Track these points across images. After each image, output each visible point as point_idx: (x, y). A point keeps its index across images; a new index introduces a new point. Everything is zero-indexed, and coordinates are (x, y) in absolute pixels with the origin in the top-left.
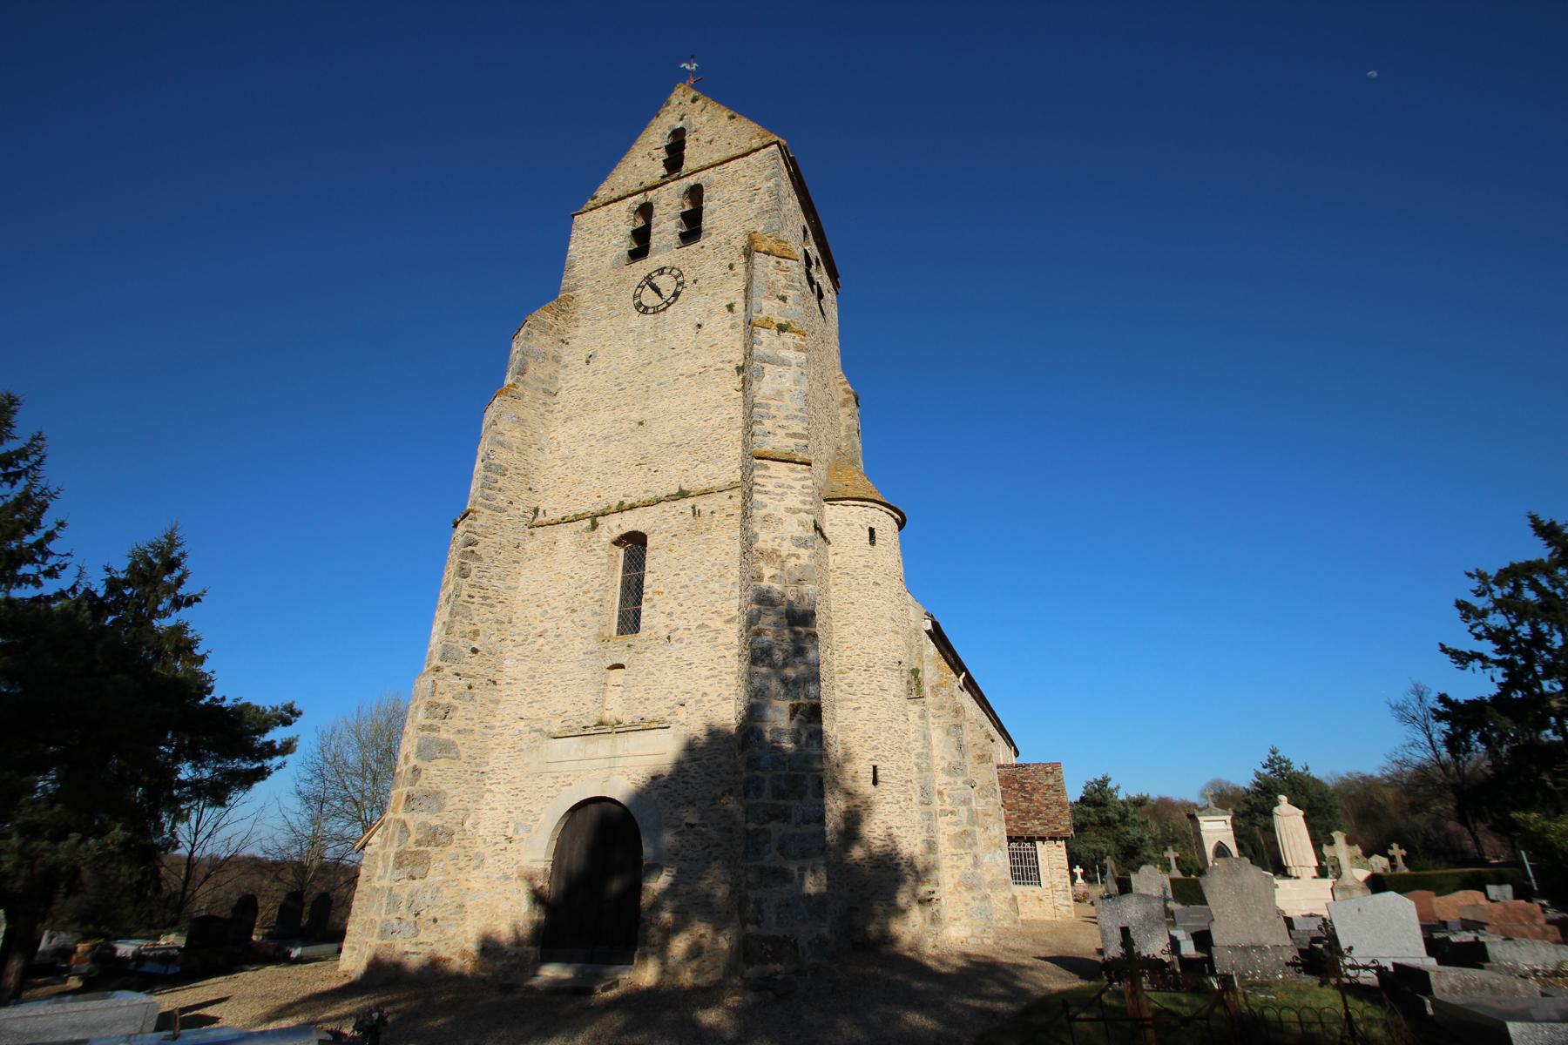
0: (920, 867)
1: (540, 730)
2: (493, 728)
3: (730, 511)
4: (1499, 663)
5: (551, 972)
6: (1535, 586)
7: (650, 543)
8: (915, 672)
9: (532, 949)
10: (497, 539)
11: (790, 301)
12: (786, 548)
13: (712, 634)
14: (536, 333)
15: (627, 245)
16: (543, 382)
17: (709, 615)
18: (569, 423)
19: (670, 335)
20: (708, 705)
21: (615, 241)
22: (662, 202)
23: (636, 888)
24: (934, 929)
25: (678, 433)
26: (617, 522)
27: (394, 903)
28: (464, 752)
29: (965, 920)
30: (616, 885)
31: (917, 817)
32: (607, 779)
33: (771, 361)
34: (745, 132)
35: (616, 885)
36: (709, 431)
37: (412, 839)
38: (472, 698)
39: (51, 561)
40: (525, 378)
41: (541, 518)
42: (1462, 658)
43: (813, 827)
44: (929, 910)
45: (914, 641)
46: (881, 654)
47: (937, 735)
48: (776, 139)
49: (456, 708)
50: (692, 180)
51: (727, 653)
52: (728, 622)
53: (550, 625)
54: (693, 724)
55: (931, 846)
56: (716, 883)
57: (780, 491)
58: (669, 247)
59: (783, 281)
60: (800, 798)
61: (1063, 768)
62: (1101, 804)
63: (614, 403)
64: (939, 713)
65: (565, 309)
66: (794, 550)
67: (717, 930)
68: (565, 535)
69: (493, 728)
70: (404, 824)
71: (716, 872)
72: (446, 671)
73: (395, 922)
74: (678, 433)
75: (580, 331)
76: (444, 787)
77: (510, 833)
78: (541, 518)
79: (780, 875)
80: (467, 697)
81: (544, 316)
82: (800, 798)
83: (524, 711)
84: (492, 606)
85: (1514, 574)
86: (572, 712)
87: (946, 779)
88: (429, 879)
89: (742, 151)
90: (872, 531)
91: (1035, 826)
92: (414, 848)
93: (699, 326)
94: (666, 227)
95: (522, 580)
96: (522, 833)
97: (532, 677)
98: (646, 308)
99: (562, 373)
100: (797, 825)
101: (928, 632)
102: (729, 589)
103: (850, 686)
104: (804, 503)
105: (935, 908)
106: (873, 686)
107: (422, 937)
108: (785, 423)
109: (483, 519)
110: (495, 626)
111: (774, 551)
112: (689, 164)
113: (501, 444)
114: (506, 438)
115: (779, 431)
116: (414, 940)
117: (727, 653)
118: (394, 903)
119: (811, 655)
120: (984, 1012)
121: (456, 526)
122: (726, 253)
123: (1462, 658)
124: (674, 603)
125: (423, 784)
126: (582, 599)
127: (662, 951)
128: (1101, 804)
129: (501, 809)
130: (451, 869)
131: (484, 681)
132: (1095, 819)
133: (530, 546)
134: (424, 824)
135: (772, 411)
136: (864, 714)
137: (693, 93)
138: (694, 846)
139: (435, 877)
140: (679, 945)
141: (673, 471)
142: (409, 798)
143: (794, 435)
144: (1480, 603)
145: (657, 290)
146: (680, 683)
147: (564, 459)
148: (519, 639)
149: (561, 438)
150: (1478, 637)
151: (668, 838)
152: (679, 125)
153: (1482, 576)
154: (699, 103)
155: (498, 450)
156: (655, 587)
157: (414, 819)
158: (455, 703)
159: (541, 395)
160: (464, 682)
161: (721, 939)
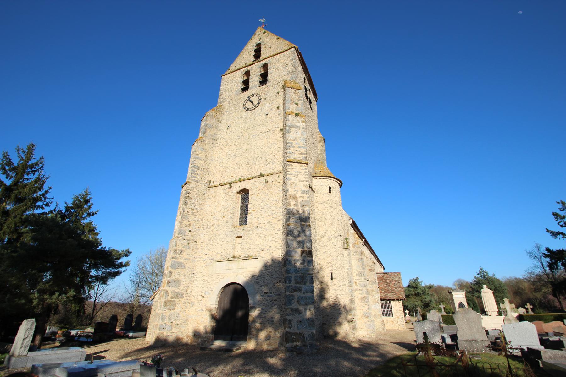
0: (348, 308)
2: (197, 258)
5: (218, 343)
9: (211, 335)
10: (197, 192)
14: (209, 118)
16: (212, 136)
17: (271, 218)
19: (256, 118)
21: (237, 85)
22: (253, 70)
23: (247, 315)
24: (354, 332)
27: (164, 318)
28: (187, 266)
31: (347, 291)
34: (283, 44)
35: (240, 313)
37: (170, 296)
38: (189, 248)
39: (47, 200)
40: (206, 135)
41: (212, 184)
44: (352, 325)
45: (346, 228)
46: (333, 232)
48: (294, 46)
49: (184, 251)
50: (264, 62)
51: (278, 232)
52: (278, 221)
54: (266, 257)
55: (352, 301)
57: (296, 174)
59: (297, 98)
60: (305, 284)
61: (401, 274)
62: (415, 288)
63: (237, 143)
64: (355, 254)
66: (302, 195)
68: (221, 190)
69: (197, 258)
72: (180, 238)
73: (164, 325)
75: (225, 118)
76: (180, 278)
77: (203, 295)
78: (212, 184)
79: (298, 311)
81: (212, 112)
82: (305, 284)
83: (207, 252)
87: (358, 278)
88: (176, 310)
90: (330, 188)
91: (390, 295)
92: (170, 300)
94: (255, 79)
96: (207, 295)
97: (210, 240)
99: (219, 133)
100: (304, 293)
101: (351, 225)
102: (279, 209)
103: (322, 244)
104: (305, 178)
105: (354, 324)
106: (331, 244)
107: (174, 330)
108: (298, 149)
109: (192, 185)
112: (263, 56)
113: (198, 158)
114: (200, 156)
115: (296, 152)
117: (278, 232)
118: (164, 318)
125: (173, 277)
127: (256, 337)
128: (415, 288)
131: (193, 242)
132: (413, 293)
133: (208, 194)
134: (173, 291)
135: (294, 145)
136: (327, 254)
137: (264, 30)
139: (177, 309)
140: (262, 335)
142: (168, 282)
143: (302, 154)
145: (252, 102)
148: (205, 227)
149: (218, 156)
150: (562, 226)
151: (258, 297)
152: (259, 42)
154: (266, 34)
155: (197, 160)
156: (252, 208)
157: (170, 289)
158: (184, 249)
159: (211, 141)
160: (187, 242)
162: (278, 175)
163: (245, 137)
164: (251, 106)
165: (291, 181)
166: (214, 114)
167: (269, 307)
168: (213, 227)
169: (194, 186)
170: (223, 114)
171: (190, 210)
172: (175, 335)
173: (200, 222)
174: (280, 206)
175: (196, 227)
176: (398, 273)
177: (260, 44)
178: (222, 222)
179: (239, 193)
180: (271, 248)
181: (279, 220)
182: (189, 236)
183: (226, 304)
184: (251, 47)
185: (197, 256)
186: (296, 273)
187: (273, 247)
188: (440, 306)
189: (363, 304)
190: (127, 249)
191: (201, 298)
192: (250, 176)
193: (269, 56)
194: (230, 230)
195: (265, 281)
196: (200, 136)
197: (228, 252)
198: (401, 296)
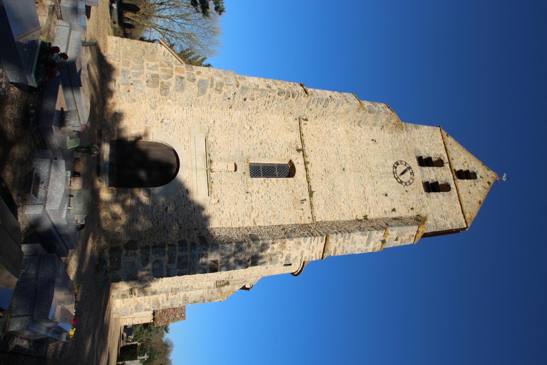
0: (146, 289)
1: (209, 132)
2: (211, 108)
3: (303, 218)
5: (106, 149)
8: (228, 283)
9: (116, 137)
10: (295, 106)
11: (395, 242)
12: (286, 252)
13: (249, 213)
14: (387, 116)
15: (425, 155)
16: (365, 120)
18: (345, 133)
19: (383, 181)
20: (218, 214)
21: (427, 149)
22: (443, 171)
23: (141, 185)
24: (120, 296)
25: (339, 189)
26: (300, 162)
27: (137, 75)
28: (201, 98)
29: (123, 305)
30: (143, 174)
31: (166, 287)
32: (187, 167)
33: (369, 239)
34: (472, 210)
35: (143, 174)
36: (339, 204)
37: (164, 80)
40: (367, 113)
41: (303, 122)
43: (166, 273)
44: (128, 293)
45: (241, 281)
47: (201, 292)
48: (469, 225)
50: (453, 186)
51: (240, 221)
52: (254, 221)
53: (255, 132)
54: (210, 210)
55: (154, 293)
56: (144, 224)
57: (311, 248)
58: (423, 176)
60: (178, 267)
61: (183, 321)
63: (353, 155)
65: (398, 127)
66: (285, 255)
67: (123, 226)
68: (294, 136)
69: (211, 108)
70: (170, 77)
71: (147, 223)
72: (237, 89)
73: (129, 76)
74: (339, 188)
75: (387, 135)
76: (186, 91)
78: (303, 122)
79: (146, 262)
80: (225, 98)
81: (395, 118)
82: (178, 267)
83: (218, 122)
84: (265, 105)
86: (217, 147)
87: (182, 296)
89: (464, 208)
92: (160, 81)
93: (386, 195)
94: (432, 174)
95: (276, 116)
97: (232, 124)
98: (396, 167)
99: (368, 127)
100: (166, 267)
102: (269, 220)
104: (306, 258)
105: (129, 296)
107: (122, 87)
108: (341, 246)
109: (304, 99)
110: (255, 107)
111: (285, 248)
112: (460, 182)
113: (338, 105)
115: (338, 244)
116: (121, 84)
117: (240, 221)
118: (137, 75)
119: (239, 267)
121: (301, 85)
122: (419, 206)
124: (263, 194)
125: (187, 83)
126: (266, 148)
127: (116, 201)
129: (175, 115)
130: (151, 96)
131: (231, 104)
133: (291, 118)
134: (170, 84)
135: (346, 241)
137: (492, 182)
138: (158, 212)
139: (147, 90)
140: (117, 209)
141: (321, 187)
142: (182, 78)
145: (402, 173)
146: (228, 199)
147: (329, 132)
148: (249, 117)
149: (339, 129)
151: (162, 199)
152: (478, 176)
154: (488, 185)
155: (335, 104)
156: (271, 184)
157: (173, 81)
158: (223, 93)
161: (119, 228)
162: (311, 216)
163: (361, 166)
165: (302, 242)
166: (392, 121)
168: (248, 128)
169: (300, 104)
170: (392, 133)
171: (272, 98)
172: (116, 88)
173: (256, 111)
174: (273, 222)
175: (250, 106)
176: (184, 318)
177: (475, 178)
178: (255, 141)
179: (291, 161)
180: (221, 212)
181: (255, 223)
182: (239, 99)
183: (155, 154)
184: (473, 165)
185: (213, 108)
186: (191, 256)
187: (222, 217)
188: (146, 355)
189: (151, 303)
190: (225, 10)
191: (160, 119)
192: (311, 177)
193: (460, 192)
194: (244, 153)
195: (181, 207)
196: (366, 104)
197: (217, 153)
198: (158, 323)
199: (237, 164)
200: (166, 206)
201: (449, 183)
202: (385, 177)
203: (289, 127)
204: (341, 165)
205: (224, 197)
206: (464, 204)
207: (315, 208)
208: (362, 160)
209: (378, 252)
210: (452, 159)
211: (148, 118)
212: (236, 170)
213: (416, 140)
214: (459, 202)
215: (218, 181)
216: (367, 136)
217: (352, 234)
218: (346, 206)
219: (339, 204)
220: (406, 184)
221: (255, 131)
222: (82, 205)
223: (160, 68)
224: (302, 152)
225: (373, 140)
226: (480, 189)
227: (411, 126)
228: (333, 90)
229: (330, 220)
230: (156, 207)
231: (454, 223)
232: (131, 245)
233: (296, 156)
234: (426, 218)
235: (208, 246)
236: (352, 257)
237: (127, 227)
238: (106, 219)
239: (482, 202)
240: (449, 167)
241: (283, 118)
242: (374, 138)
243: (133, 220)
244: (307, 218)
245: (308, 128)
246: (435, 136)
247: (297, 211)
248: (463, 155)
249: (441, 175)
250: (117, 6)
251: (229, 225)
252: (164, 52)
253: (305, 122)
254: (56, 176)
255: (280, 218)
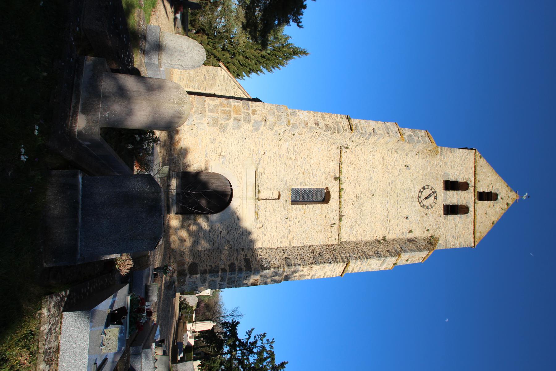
3: (330, 239)
4: (247, 342)
6: (267, 358)
7: (325, 206)
10: (338, 138)
13: (286, 236)
15: (452, 178)
17: (293, 234)
18: (381, 159)
19: (407, 205)
21: (456, 173)
22: (466, 195)
34: (484, 228)
35: (203, 202)
37: (223, 122)
41: (344, 150)
42: (249, 333)
50: (471, 209)
52: (290, 242)
53: (299, 163)
54: (256, 235)
56: (204, 245)
57: (333, 270)
63: (385, 181)
68: (335, 165)
72: (288, 128)
75: (421, 160)
76: (242, 129)
78: (344, 150)
85: (272, 355)
86: (265, 177)
92: (219, 123)
94: (455, 198)
97: (280, 155)
99: (404, 153)
108: (358, 267)
111: (312, 270)
112: (480, 203)
120: (163, 304)
123: (249, 333)
124: (300, 219)
126: (307, 177)
127: (182, 227)
133: (333, 147)
134: (228, 124)
137: (511, 203)
138: (214, 235)
139: (208, 129)
140: (184, 234)
144: (265, 340)
148: (296, 148)
149: (376, 156)
150: (255, 337)
151: (217, 225)
152: (499, 197)
153: (272, 342)
154: (506, 206)
156: (307, 210)
158: (274, 131)
160: (282, 132)
162: (337, 238)
164: (425, 196)
167: (208, 238)
168: (294, 158)
174: (305, 242)
178: (299, 171)
181: (290, 244)
182: (289, 133)
184: (497, 187)
191: (218, 152)
192: (343, 203)
194: (288, 183)
195: (232, 231)
196: (407, 132)
197: (265, 183)
199: (281, 193)
200: (220, 230)
201: (469, 205)
202: (409, 201)
203: (330, 156)
204: (371, 191)
205: (268, 222)
206: (477, 225)
207: (342, 230)
208: (391, 185)
209: (389, 270)
210: (479, 181)
211: (208, 152)
212: (279, 198)
213: (448, 164)
214: (473, 224)
215: (263, 208)
216: (401, 162)
217: (369, 260)
218: (369, 228)
219: (363, 226)
220: (427, 208)
221: (299, 162)
222: (163, 366)
223: (220, 108)
224: (338, 180)
225: (405, 166)
226: (498, 210)
227: (447, 150)
228: (376, 119)
229: (353, 240)
230: (212, 231)
231: (463, 242)
232: (193, 269)
233: (332, 184)
234: (438, 238)
235: (251, 271)
236: (367, 273)
237: (192, 251)
238: (174, 242)
239: (495, 222)
240: (473, 191)
241: (326, 147)
242: (407, 164)
243: (196, 243)
244: (334, 239)
245: (347, 156)
246: (468, 159)
247: (327, 233)
248: (490, 177)
249: (463, 198)
250: (181, 16)
251: (269, 245)
252: (224, 77)
253: (346, 150)
254: (146, 365)
255: (311, 240)
